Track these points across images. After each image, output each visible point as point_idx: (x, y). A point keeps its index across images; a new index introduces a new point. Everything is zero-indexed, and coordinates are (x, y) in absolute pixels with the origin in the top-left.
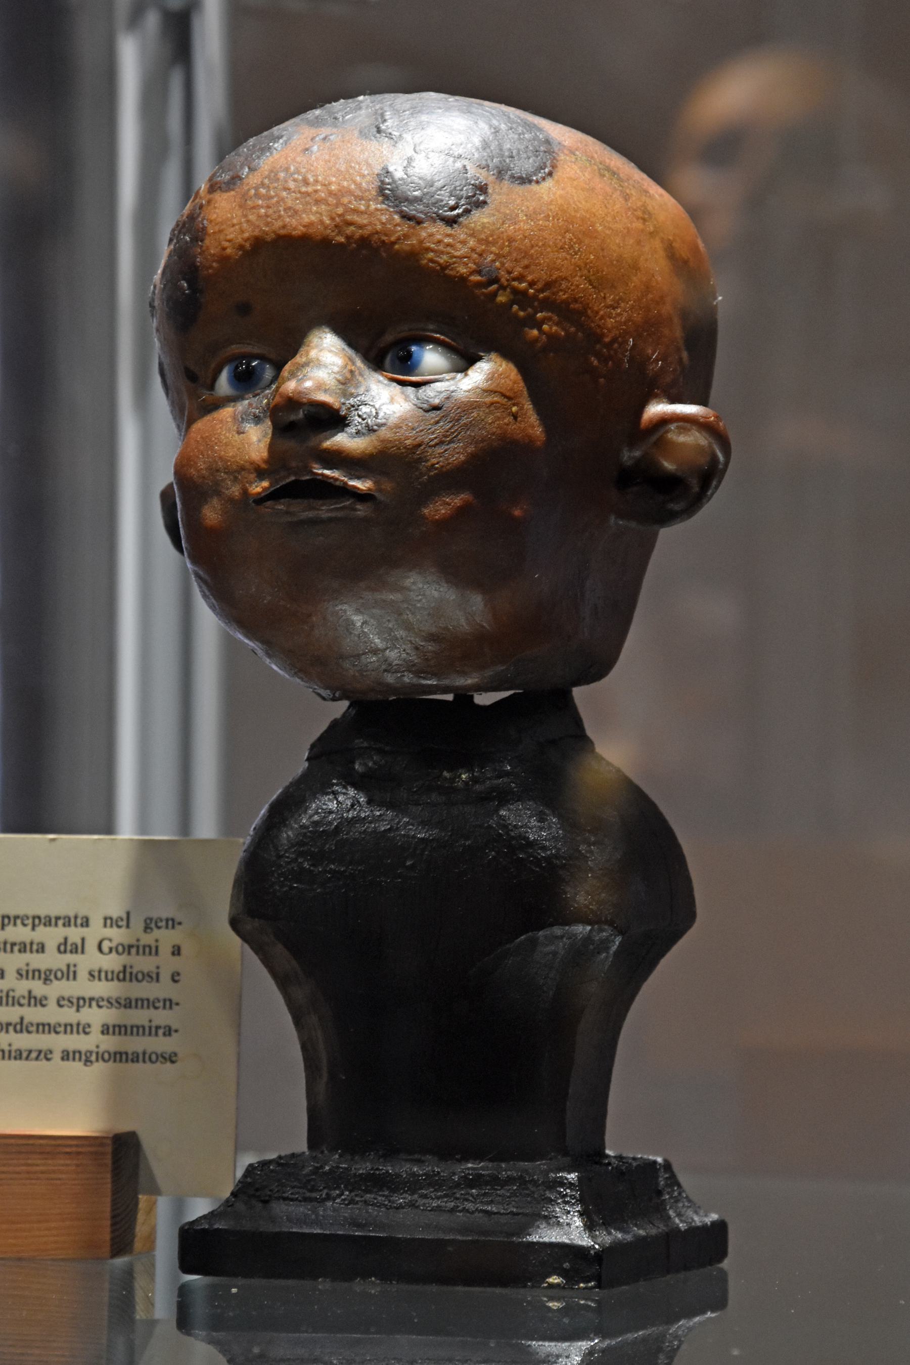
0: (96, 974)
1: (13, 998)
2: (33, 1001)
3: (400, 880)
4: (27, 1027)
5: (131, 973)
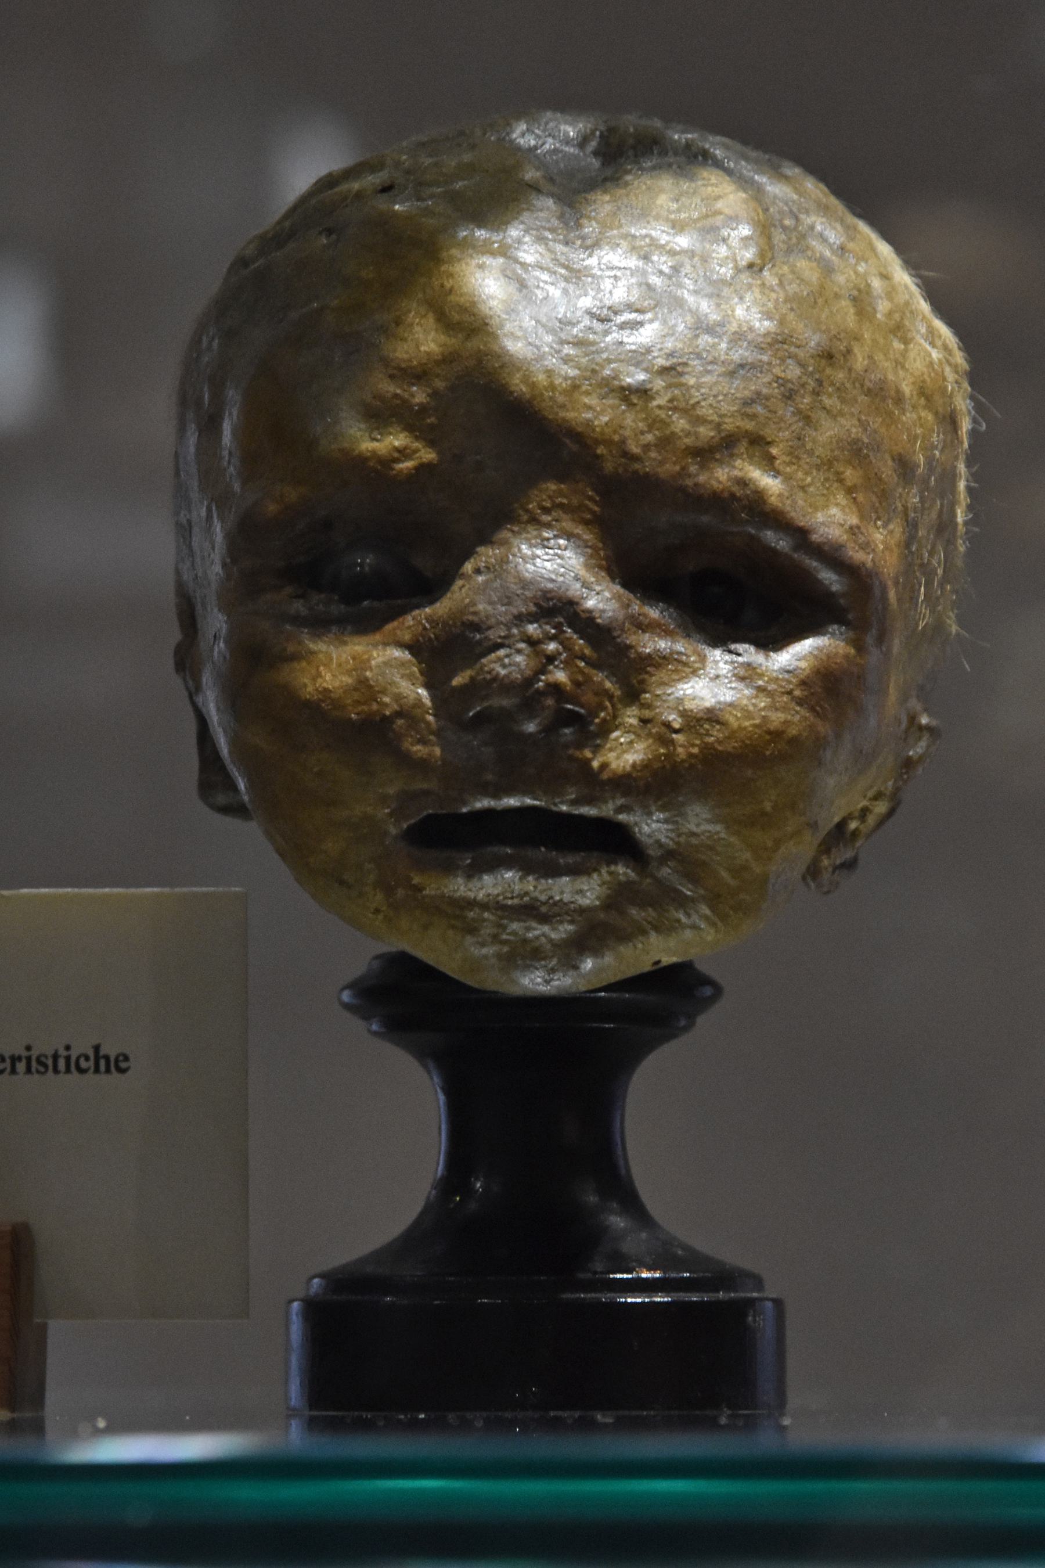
0: (50, 1062)
1: (68, 1059)
2: (102, 1063)
3: (436, 1302)
4: (117, 1061)
5: (68, 1059)
